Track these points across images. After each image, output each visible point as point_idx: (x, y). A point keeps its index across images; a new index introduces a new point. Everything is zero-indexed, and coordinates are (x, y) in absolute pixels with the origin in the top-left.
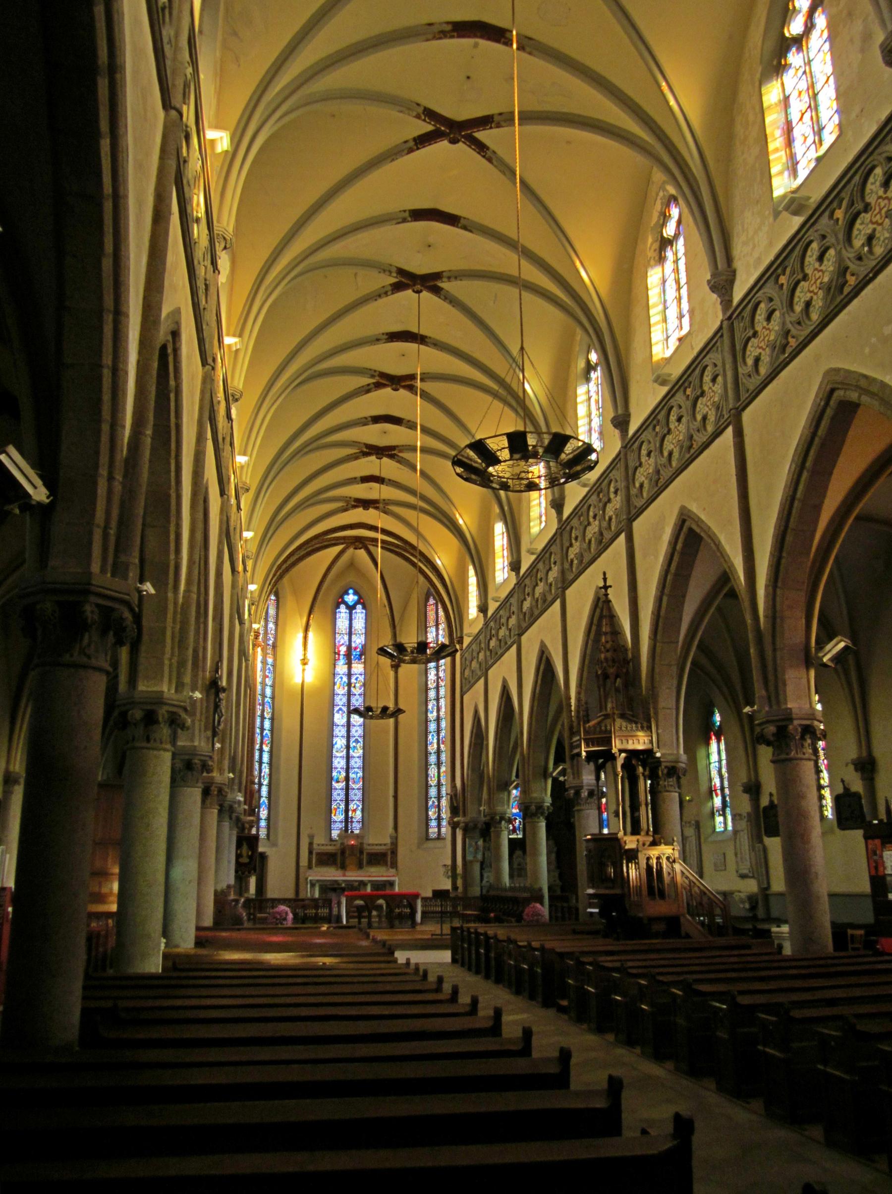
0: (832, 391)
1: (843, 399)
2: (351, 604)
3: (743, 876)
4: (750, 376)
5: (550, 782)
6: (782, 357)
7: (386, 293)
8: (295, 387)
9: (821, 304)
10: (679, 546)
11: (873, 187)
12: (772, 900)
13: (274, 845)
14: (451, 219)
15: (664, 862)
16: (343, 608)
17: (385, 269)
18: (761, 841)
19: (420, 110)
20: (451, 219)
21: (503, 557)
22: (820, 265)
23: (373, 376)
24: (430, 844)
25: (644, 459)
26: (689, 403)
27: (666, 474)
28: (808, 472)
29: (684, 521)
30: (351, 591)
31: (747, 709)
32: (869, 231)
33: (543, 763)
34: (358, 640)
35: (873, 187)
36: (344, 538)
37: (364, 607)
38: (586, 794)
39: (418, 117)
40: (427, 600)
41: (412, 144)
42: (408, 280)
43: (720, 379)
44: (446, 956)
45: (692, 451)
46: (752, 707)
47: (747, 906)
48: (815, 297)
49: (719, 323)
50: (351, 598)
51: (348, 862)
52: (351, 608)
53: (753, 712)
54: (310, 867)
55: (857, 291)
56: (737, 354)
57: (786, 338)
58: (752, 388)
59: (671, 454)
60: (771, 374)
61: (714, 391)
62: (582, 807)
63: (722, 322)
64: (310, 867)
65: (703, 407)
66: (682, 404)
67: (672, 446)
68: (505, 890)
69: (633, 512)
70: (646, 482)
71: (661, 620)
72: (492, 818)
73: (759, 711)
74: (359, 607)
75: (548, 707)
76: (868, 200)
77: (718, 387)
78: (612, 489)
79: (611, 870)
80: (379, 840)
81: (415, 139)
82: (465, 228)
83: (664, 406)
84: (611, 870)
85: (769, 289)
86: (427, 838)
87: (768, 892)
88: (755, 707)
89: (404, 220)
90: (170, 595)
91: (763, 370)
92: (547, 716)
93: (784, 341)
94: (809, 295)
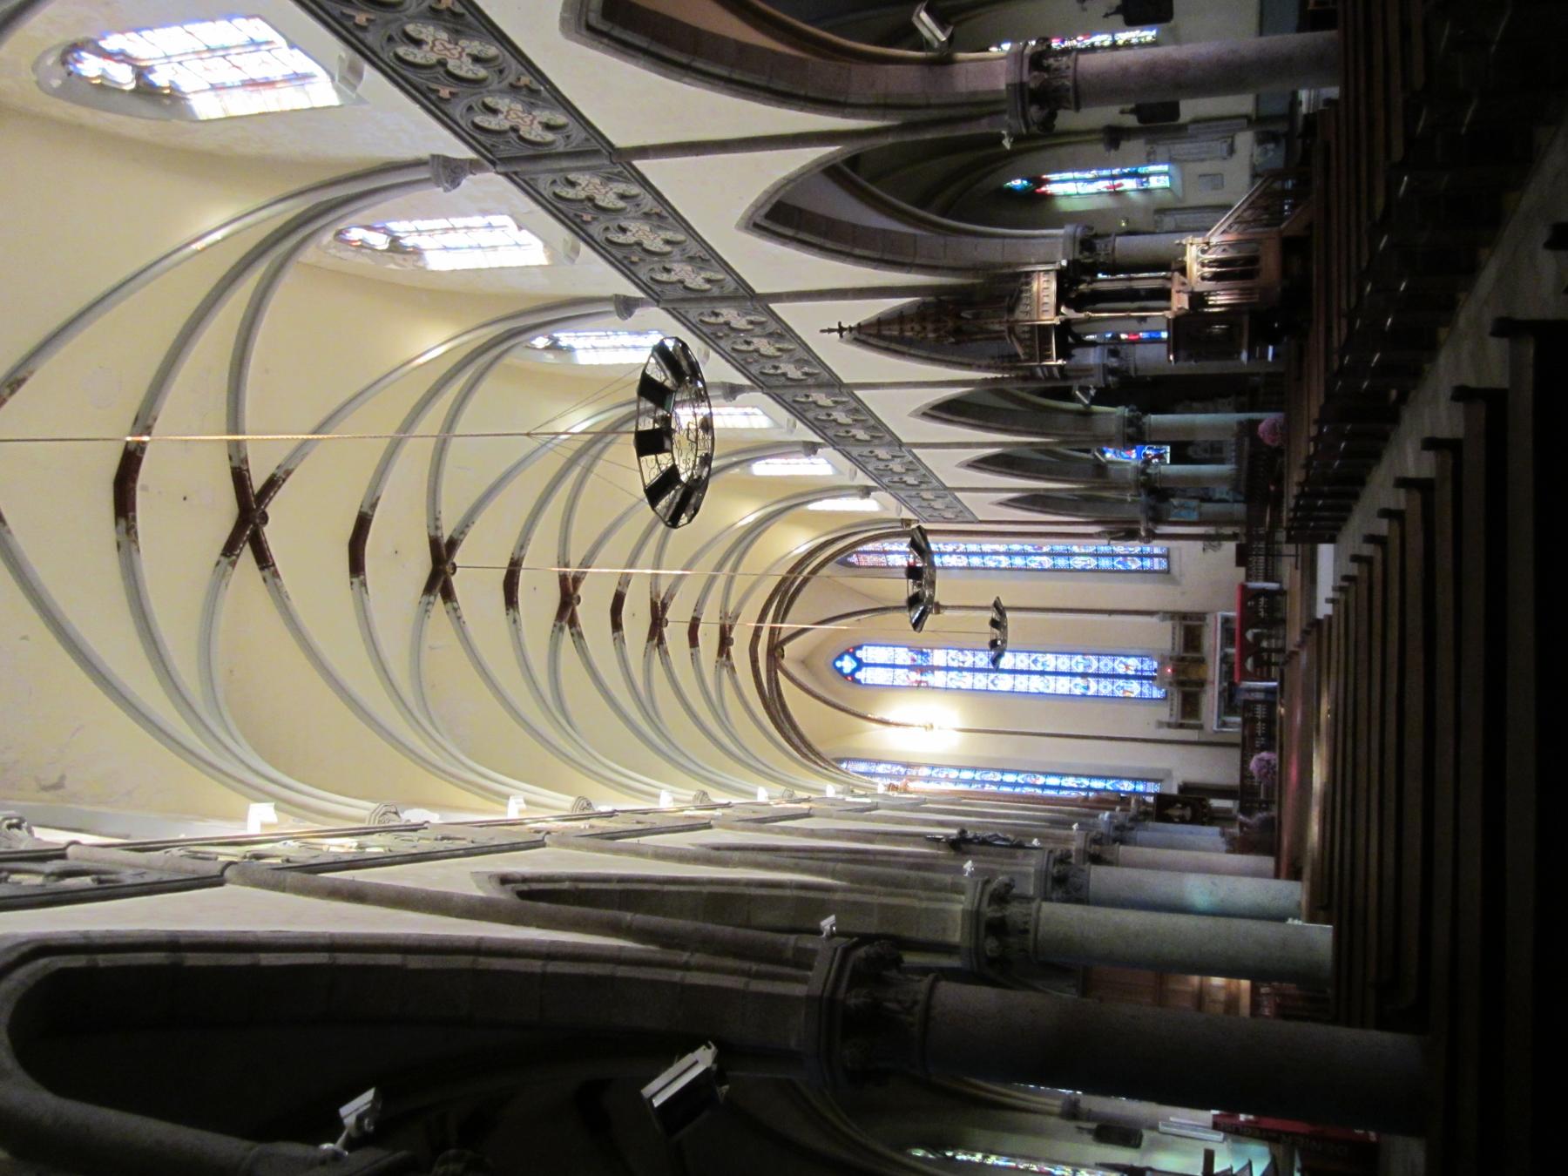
0: (590, 28)
2: (854, 665)
3: (1232, 150)
7: (456, 610)
8: (569, 722)
10: (790, 232)
13: (1169, 773)
14: (363, 524)
16: (858, 675)
18: (1184, 127)
19: (225, 561)
20: (363, 524)
23: (561, 629)
24: (1175, 569)
30: (839, 664)
31: (1007, 144)
34: (903, 656)
36: (768, 671)
37: (860, 647)
39: (233, 564)
40: (852, 565)
41: (267, 573)
42: (439, 582)
44: (1326, 552)
45: (665, 213)
47: (1271, 146)
49: (500, 177)
50: (847, 664)
51: (1194, 677)
52: (860, 664)
54: (1200, 727)
55: (710, 249)
59: (668, 242)
61: (587, 184)
64: (1200, 727)
68: (1239, 470)
72: (1143, 485)
74: (859, 654)
78: (713, 320)
80: (1164, 636)
81: (262, 569)
82: (374, 506)
86: (1168, 572)
89: (364, 584)
90: (838, 896)
93: (524, 91)
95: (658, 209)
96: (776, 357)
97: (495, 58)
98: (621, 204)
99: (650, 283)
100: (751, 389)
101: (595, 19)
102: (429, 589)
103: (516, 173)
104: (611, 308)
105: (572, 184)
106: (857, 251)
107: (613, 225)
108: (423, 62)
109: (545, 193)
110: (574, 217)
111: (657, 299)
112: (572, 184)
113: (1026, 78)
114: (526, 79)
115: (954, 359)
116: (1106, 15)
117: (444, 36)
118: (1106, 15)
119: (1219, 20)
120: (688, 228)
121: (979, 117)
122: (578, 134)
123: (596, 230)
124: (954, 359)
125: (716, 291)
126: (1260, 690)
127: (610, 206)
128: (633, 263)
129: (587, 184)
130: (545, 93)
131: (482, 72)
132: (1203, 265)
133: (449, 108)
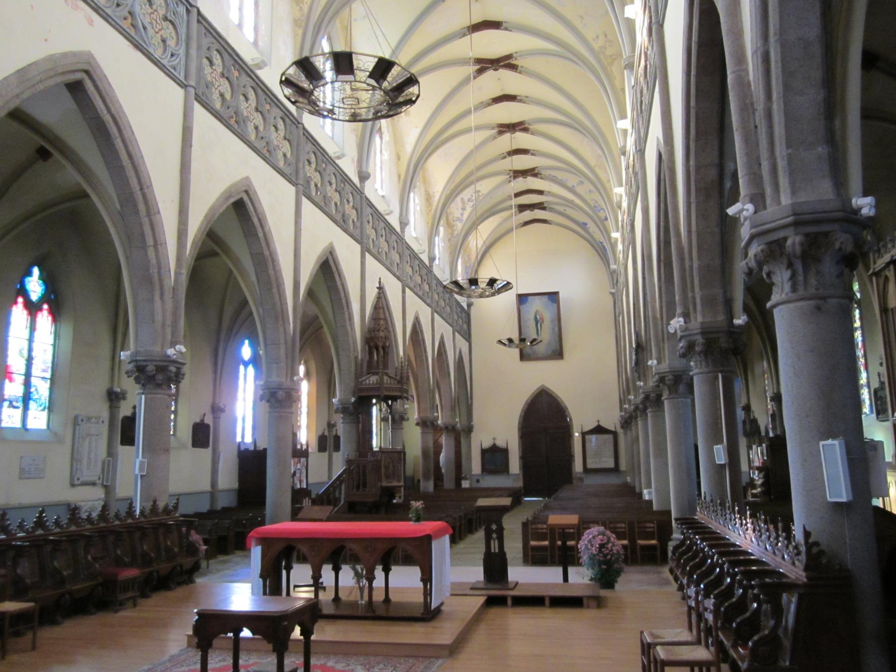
17: (464, 62)
23: (493, 128)
102: (479, 61)
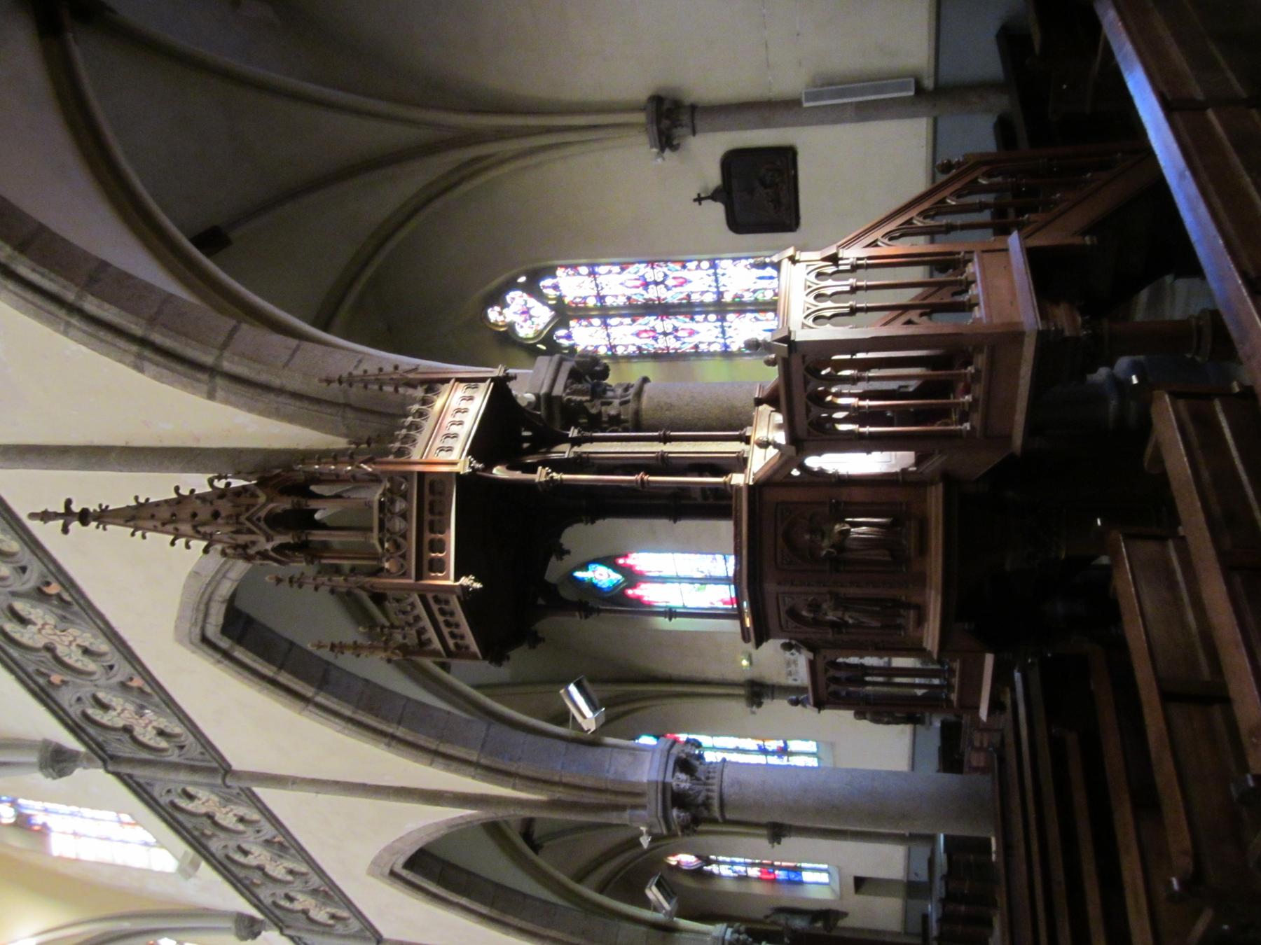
0: (205, 640)
1: (219, 629)
4: (182, 747)
5: (684, 923)
6: (337, 899)
9: (88, 635)
11: (27, 636)
12: (951, 73)
15: (831, 286)
21: (72, 814)
22: (115, 710)
25: (297, 906)
26: (222, 835)
27: (315, 881)
28: (317, 694)
29: (393, 874)
31: (645, 841)
32: (80, 652)
33: (643, 929)
35: (27, 636)
38: (683, 776)
43: (191, 789)
45: (148, 689)
46: (641, 834)
48: (79, 641)
49: (110, 776)
53: (649, 833)
55: (287, 833)
56: (154, 759)
57: (131, 688)
58: (199, 749)
59: (291, 872)
60: (180, 719)
61: (205, 800)
62: (715, 795)
63: (108, 772)
65: (228, 819)
66: (223, 843)
67: (231, 815)
69: (368, 934)
70: (329, 910)
71: (157, 338)
73: (650, 826)
75: (525, 896)
76: (40, 644)
77: (202, 794)
78: (286, 904)
79: (862, 528)
83: (225, 867)
84: (862, 528)
85: (66, 698)
87: (929, 83)
88: (643, 829)
91: (303, 868)
92: (546, 902)
93: (135, 693)
94: (73, 647)
95: (279, 839)
96: (288, 883)
97: (303, 874)
98: (331, 922)
99: (226, 862)
100: (89, 763)
101: (213, 631)
103: (131, 776)
104: (230, 924)
105: (191, 797)
106: (91, 305)
107: (232, 844)
108: (109, 724)
109: (71, 711)
110: (195, 835)
111: (107, 759)
112: (191, 797)
113: (669, 779)
114: (137, 682)
115: (400, 732)
116: (699, 199)
117: (51, 620)
118: (699, 199)
119: (908, 44)
120: (349, 904)
121: (620, 808)
122: (194, 749)
123: (215, 845)
124: (400, 732)
125: (174, 756)
126: (920, 686)
127: (279, 877)
128: (255, 884)
129: (205, 800)
130: (337, 899)
131: (90, 665)
132: (819, 297)
133: (258, 891)
